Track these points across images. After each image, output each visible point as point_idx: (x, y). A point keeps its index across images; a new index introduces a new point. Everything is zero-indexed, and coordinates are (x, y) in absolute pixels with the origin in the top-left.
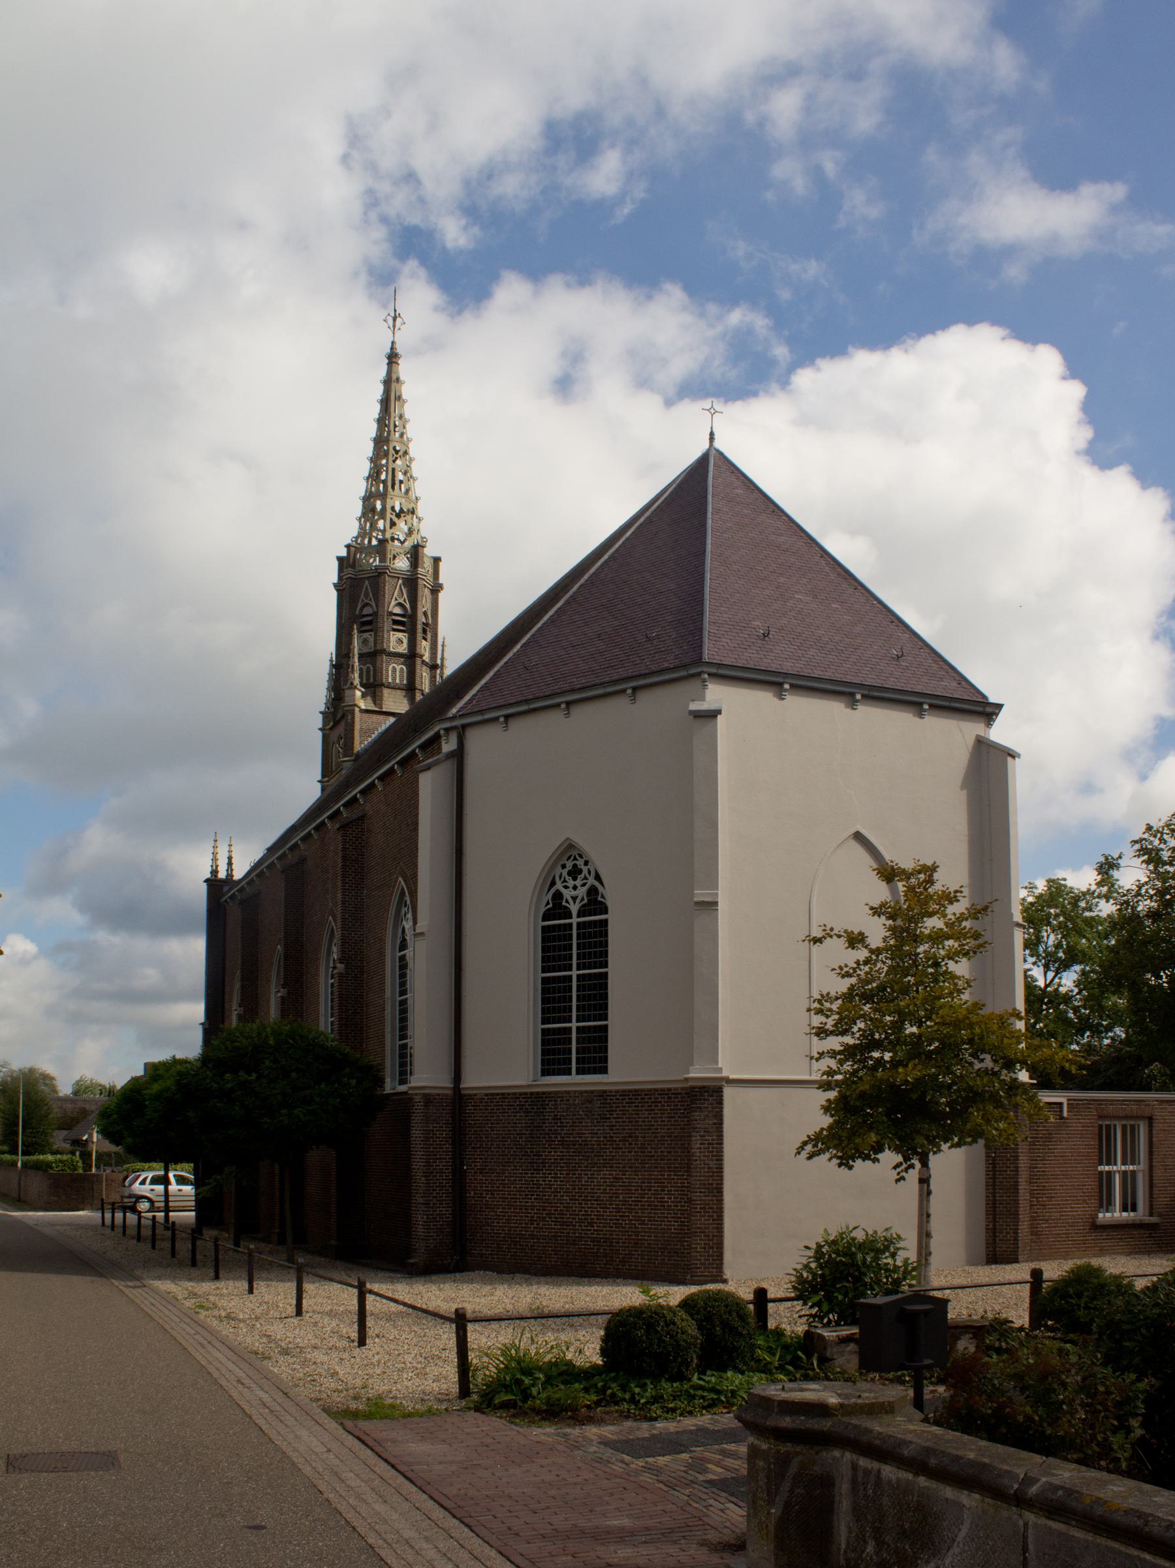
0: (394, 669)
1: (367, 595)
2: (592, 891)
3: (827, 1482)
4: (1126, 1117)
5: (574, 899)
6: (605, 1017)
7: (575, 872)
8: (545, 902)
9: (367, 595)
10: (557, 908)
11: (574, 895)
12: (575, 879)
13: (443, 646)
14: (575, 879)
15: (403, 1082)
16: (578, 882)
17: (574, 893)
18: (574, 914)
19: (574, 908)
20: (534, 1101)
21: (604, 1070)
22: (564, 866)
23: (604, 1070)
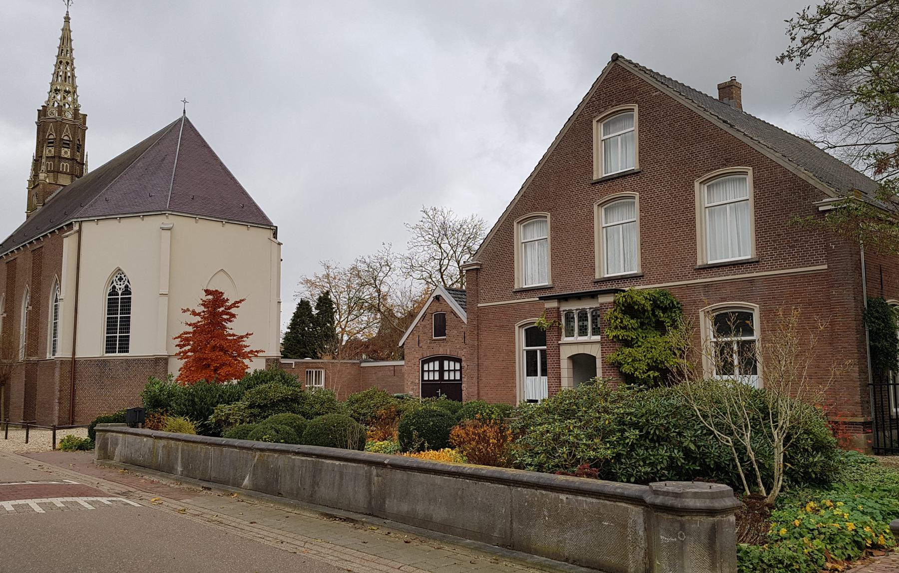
0: (63, 165)
1: (51, 130)
2: (127, 287)
3: (117, 440)
4: (316, 368)
5: (120, 289)
6: (128, 332)
7: (121, 279)
8: (109, 289)
9: (51, 130)
10: (114, 292)
11: (120, 287)
12: (120, 281)
13: (87, 156)
14: (120, 281)
15: (54, 355)
16: (122, 283)
17: (120, 287)
18: (120, 294)
19: (120, 292)
20: (101, 363)
21: (127, 352)
22: (117, 277)
23: (127, 352)
